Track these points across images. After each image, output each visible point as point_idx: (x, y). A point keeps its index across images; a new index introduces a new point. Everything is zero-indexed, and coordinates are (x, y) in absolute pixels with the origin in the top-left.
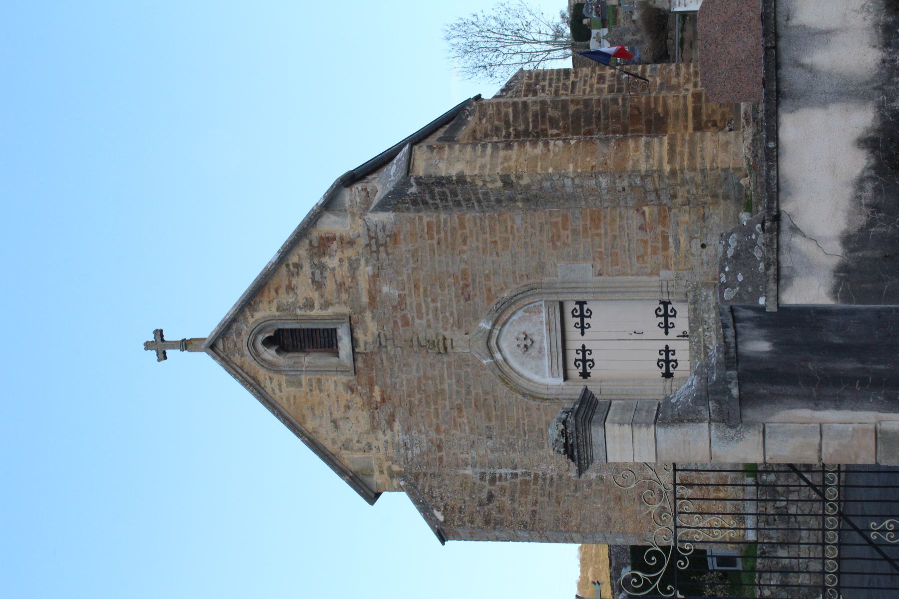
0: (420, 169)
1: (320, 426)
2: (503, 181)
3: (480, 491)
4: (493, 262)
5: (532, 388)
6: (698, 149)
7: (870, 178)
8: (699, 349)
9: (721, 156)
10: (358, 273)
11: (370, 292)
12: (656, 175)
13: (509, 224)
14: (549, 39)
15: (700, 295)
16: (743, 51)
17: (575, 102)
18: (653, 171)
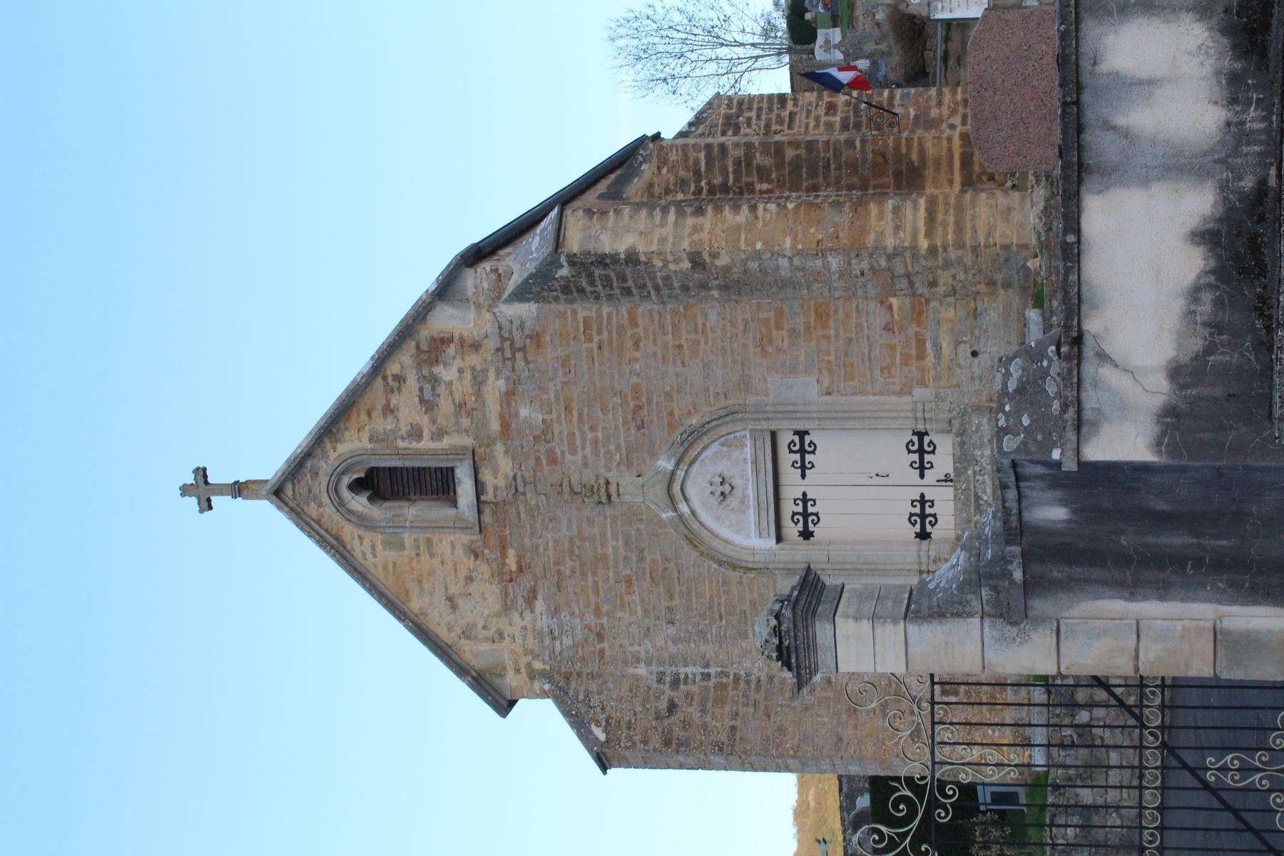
0: (574, 242)
1: (431, 604)
2: (691, 261)
3: (658, 698)
4: (677, 375)
5: (732, 554)
6: (968, 218)
7: (1209, 286)
8: (967, 499)
9: (1001, 228)
10: (485, 389)
11: (502, 417)
12: (908, 254)
13: (700, 321)
14: (757, 40)
15: (969, 422)
16: (1032, 99)
17: (795, 144)
18: (905, 249)
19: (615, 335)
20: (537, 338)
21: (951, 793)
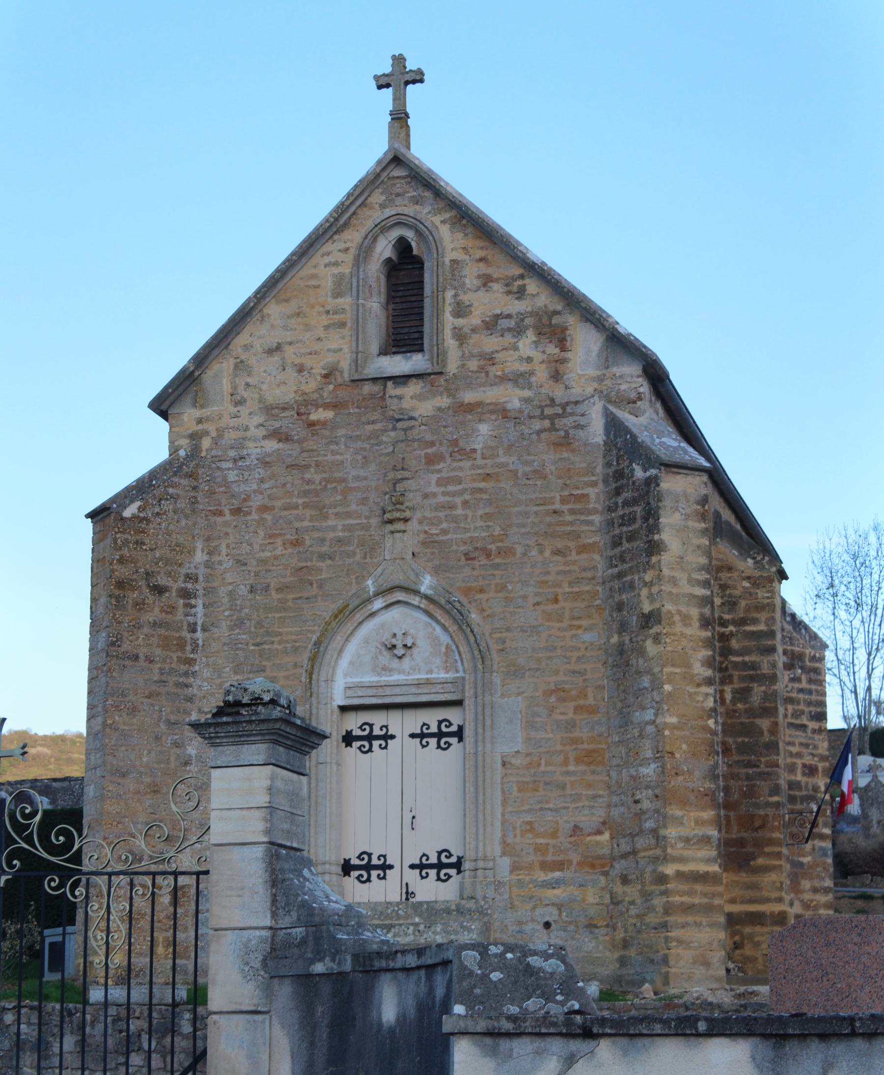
0: (671, 484)
1: (273, 326)
2: (651, 613)
3: (169, 574)
4: (525, 597)
5: (328, 656)
6: (698, 919)
8: (387, 917)
10: (510, 385)
11: (479, 404)
12: (658, 852)
13: (584, 623)
15: (472, 919)
17: (774, 729)
18: (664, 849)
19: (569, 528)
20: (565, 443)
21: (77, 893)
